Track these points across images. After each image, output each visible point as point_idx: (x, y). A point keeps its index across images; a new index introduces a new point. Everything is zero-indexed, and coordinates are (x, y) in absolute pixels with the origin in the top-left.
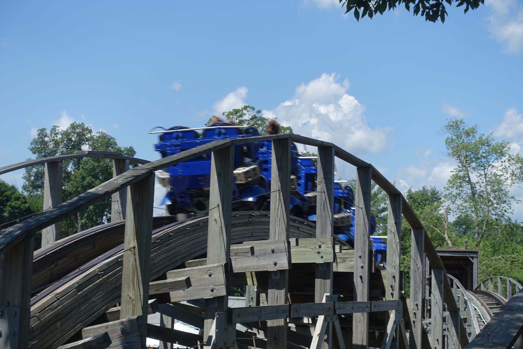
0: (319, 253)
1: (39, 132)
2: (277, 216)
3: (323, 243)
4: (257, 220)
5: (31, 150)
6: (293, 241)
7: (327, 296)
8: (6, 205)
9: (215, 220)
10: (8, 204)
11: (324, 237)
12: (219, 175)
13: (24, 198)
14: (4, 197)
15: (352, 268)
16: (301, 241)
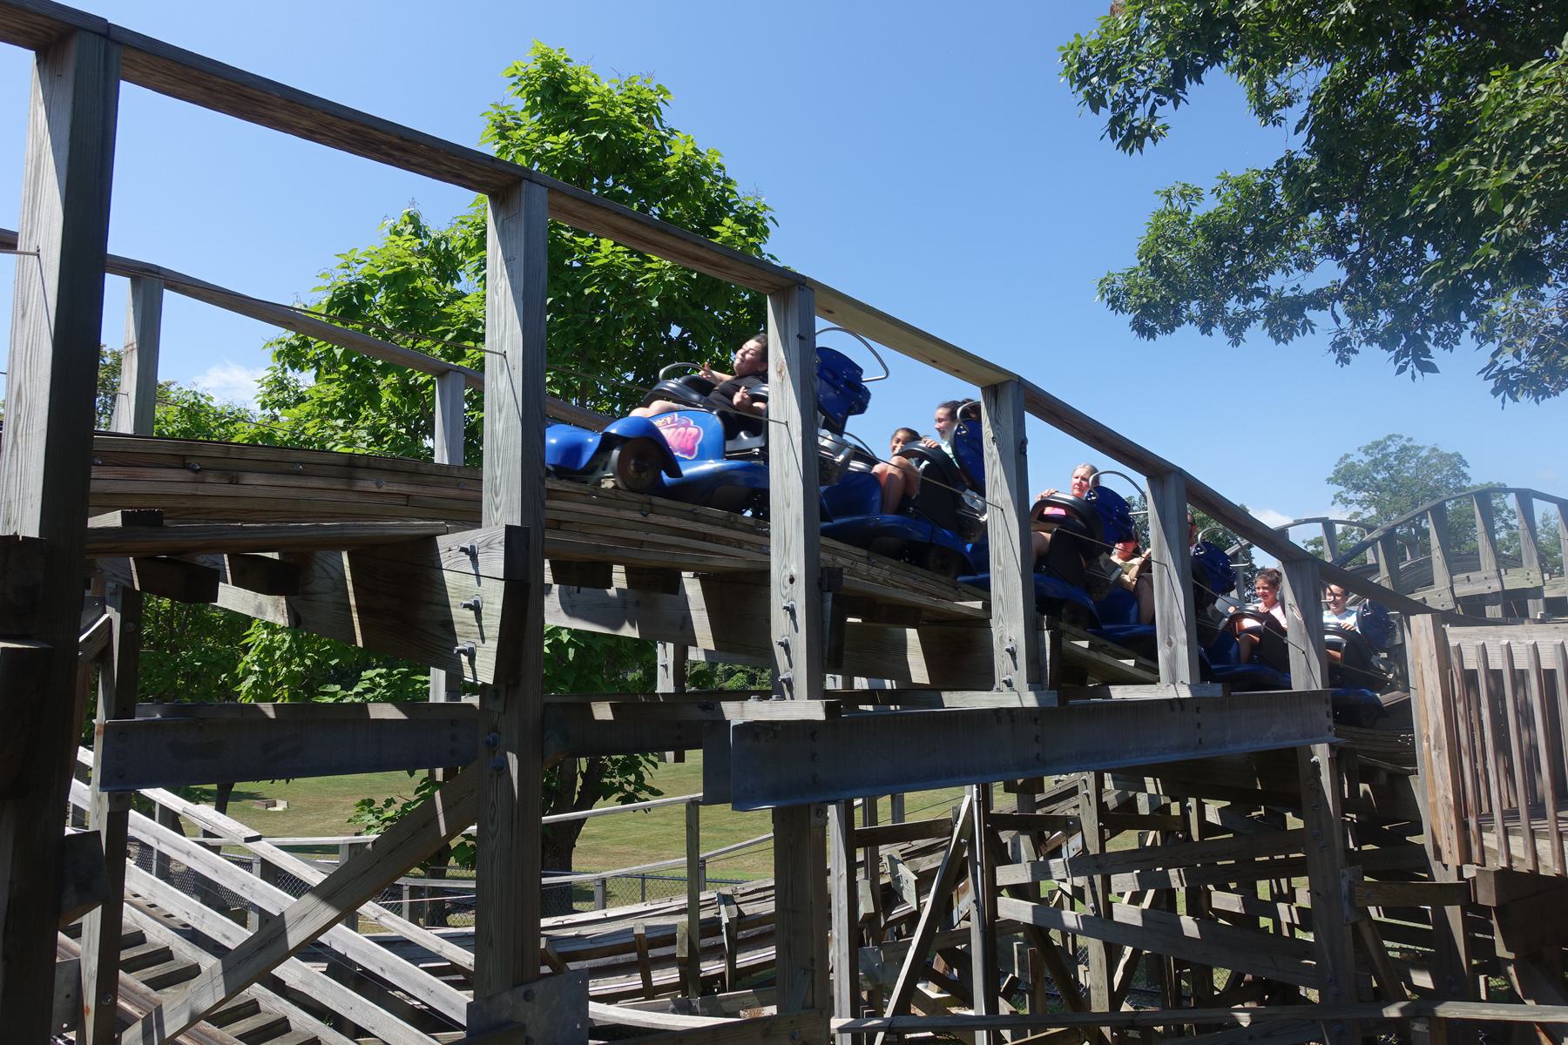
6: (1502, 571)
15: (1565, 592)
16: (1508, 571)
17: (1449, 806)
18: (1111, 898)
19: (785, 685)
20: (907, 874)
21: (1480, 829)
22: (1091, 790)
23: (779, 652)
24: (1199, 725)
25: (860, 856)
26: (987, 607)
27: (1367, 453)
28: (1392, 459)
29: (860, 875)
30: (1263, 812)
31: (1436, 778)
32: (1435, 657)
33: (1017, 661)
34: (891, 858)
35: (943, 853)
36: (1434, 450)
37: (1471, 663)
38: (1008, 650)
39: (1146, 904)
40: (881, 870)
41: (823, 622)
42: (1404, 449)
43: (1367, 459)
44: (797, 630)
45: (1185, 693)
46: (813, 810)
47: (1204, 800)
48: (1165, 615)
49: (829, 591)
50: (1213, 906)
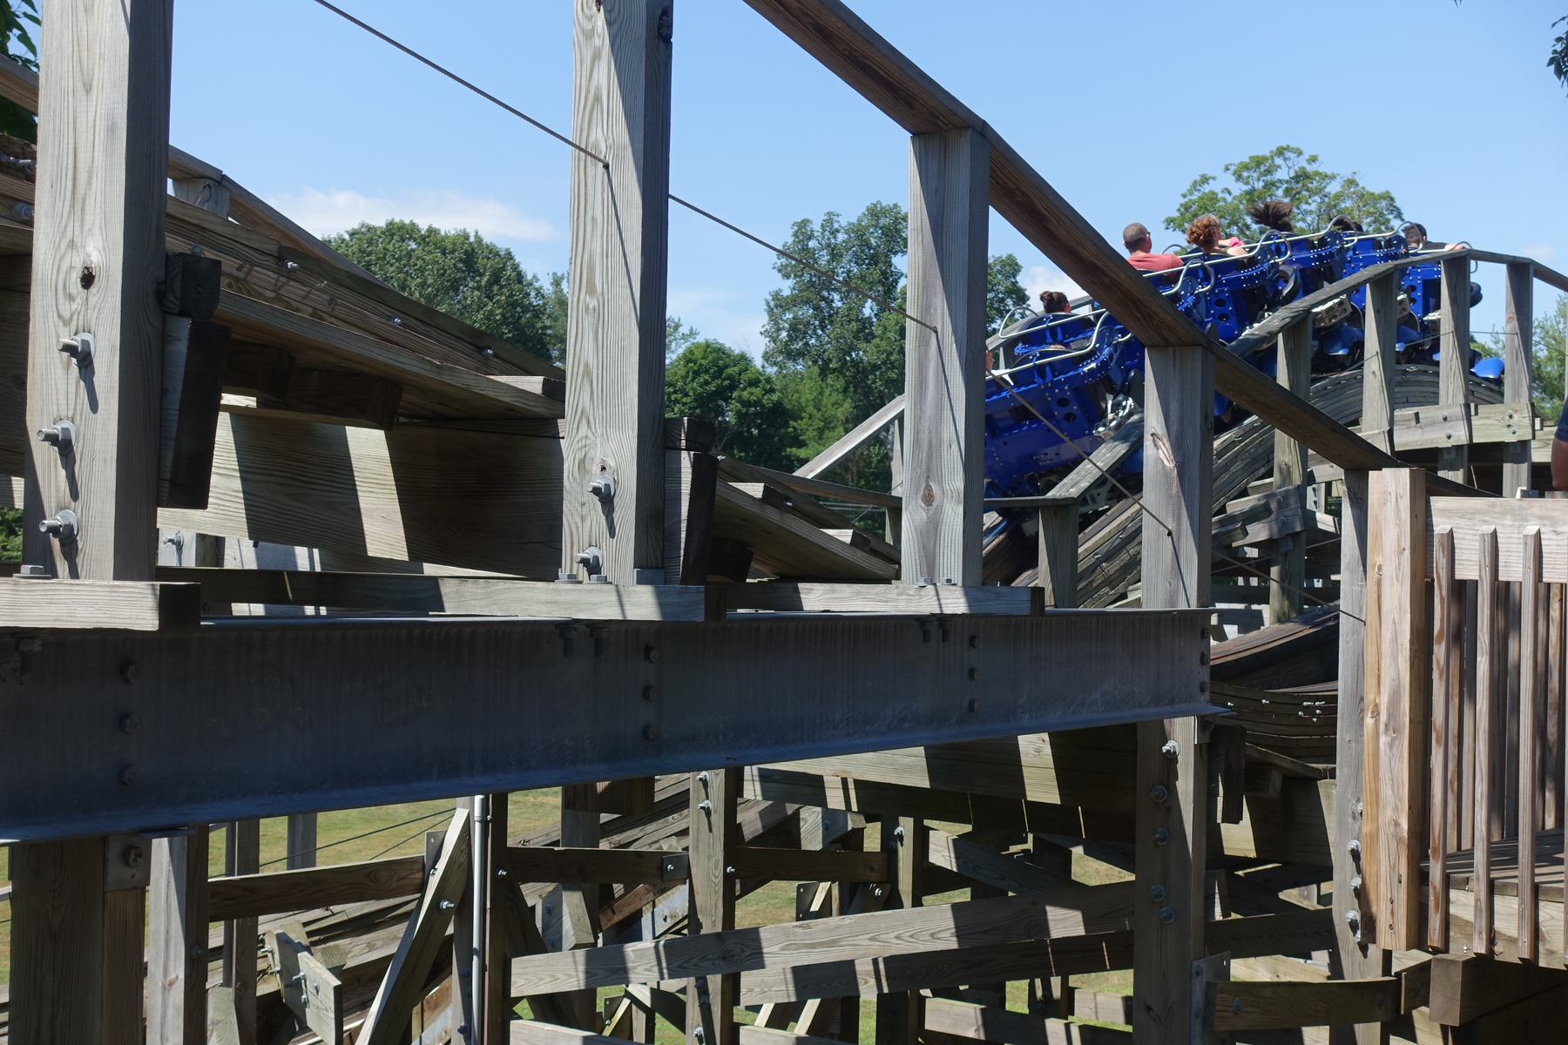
0: (1509, 426)
1: (796, 228)
2: (1451, 369)
3: (1516, 411)
4: (1413, 378)
5: (779, 271)
7: (1522, 491)
8: (730, 397)
9: (1373, 373)
10: (735, 394)
11: (1517, 401)
12: (1377, 312)
13: (768, 380)
14: (724, 380)
17: (1399, 840)
18: (739, 1014)
19: (56, 543)
20: (318, 974)
21: (1447, 883)
22: (716, 802)
23: (45, 457)
24: (971, 673)
25: (216, 935)
26: (555, 389)
27: (1239, 178)
28: (1280, 193)
29: (215, 974)
30: (1029, 845)
31: (1382, 786)
32: (1407, 553)
33: (616, 516)
34: (283, 940)
35: (400, 929)
36: (1351, 182)
37: (1469, 567)
38: (596, 491)
39: (802, 1027)
40: (261, 965)
41: (164, 391)
42: (1302, 176)
43: (1238, 189)
44: (94, 406)
45: (955, 603)
46: (114, 851)
47: (927, 822)
48: (925, 436)
49: (183, 314)
50: (928, 1026)
